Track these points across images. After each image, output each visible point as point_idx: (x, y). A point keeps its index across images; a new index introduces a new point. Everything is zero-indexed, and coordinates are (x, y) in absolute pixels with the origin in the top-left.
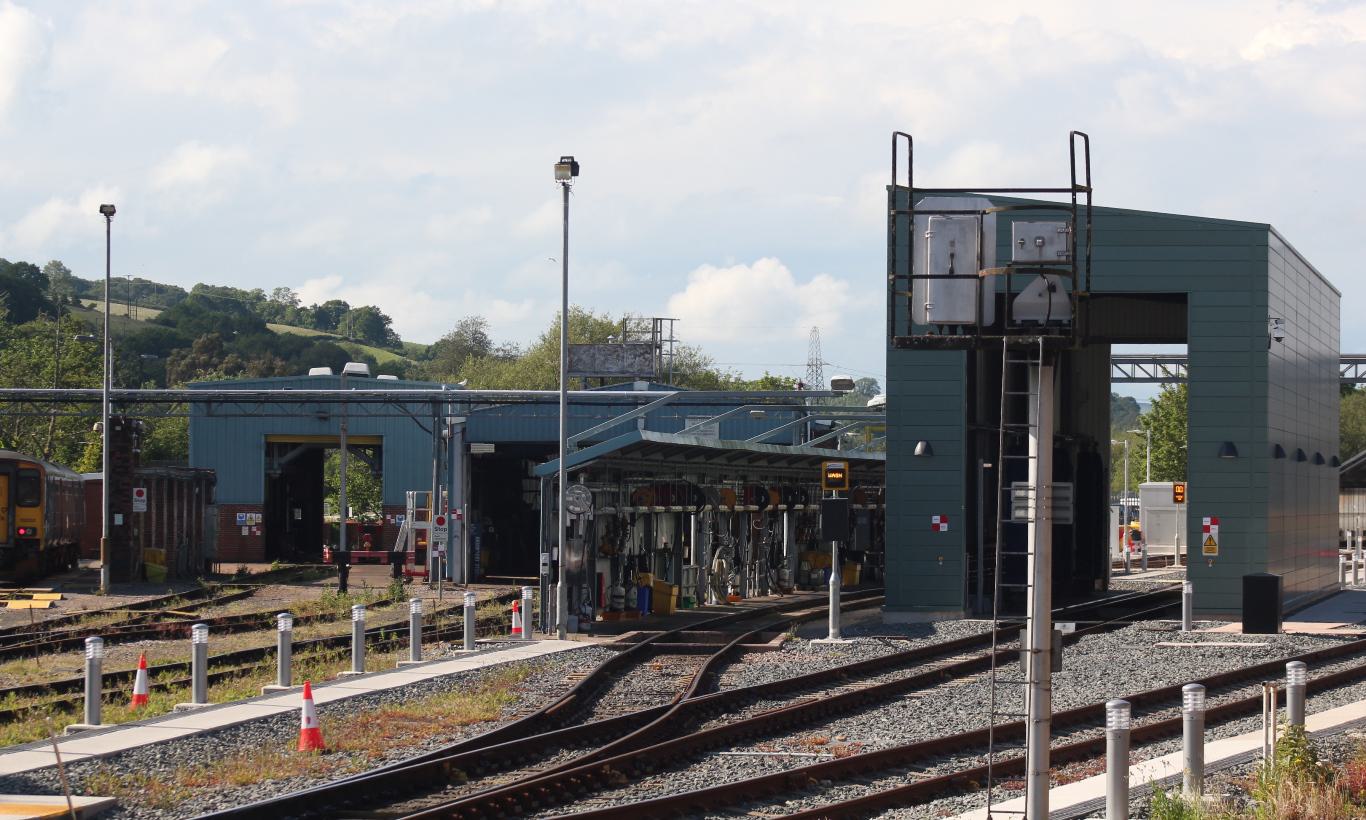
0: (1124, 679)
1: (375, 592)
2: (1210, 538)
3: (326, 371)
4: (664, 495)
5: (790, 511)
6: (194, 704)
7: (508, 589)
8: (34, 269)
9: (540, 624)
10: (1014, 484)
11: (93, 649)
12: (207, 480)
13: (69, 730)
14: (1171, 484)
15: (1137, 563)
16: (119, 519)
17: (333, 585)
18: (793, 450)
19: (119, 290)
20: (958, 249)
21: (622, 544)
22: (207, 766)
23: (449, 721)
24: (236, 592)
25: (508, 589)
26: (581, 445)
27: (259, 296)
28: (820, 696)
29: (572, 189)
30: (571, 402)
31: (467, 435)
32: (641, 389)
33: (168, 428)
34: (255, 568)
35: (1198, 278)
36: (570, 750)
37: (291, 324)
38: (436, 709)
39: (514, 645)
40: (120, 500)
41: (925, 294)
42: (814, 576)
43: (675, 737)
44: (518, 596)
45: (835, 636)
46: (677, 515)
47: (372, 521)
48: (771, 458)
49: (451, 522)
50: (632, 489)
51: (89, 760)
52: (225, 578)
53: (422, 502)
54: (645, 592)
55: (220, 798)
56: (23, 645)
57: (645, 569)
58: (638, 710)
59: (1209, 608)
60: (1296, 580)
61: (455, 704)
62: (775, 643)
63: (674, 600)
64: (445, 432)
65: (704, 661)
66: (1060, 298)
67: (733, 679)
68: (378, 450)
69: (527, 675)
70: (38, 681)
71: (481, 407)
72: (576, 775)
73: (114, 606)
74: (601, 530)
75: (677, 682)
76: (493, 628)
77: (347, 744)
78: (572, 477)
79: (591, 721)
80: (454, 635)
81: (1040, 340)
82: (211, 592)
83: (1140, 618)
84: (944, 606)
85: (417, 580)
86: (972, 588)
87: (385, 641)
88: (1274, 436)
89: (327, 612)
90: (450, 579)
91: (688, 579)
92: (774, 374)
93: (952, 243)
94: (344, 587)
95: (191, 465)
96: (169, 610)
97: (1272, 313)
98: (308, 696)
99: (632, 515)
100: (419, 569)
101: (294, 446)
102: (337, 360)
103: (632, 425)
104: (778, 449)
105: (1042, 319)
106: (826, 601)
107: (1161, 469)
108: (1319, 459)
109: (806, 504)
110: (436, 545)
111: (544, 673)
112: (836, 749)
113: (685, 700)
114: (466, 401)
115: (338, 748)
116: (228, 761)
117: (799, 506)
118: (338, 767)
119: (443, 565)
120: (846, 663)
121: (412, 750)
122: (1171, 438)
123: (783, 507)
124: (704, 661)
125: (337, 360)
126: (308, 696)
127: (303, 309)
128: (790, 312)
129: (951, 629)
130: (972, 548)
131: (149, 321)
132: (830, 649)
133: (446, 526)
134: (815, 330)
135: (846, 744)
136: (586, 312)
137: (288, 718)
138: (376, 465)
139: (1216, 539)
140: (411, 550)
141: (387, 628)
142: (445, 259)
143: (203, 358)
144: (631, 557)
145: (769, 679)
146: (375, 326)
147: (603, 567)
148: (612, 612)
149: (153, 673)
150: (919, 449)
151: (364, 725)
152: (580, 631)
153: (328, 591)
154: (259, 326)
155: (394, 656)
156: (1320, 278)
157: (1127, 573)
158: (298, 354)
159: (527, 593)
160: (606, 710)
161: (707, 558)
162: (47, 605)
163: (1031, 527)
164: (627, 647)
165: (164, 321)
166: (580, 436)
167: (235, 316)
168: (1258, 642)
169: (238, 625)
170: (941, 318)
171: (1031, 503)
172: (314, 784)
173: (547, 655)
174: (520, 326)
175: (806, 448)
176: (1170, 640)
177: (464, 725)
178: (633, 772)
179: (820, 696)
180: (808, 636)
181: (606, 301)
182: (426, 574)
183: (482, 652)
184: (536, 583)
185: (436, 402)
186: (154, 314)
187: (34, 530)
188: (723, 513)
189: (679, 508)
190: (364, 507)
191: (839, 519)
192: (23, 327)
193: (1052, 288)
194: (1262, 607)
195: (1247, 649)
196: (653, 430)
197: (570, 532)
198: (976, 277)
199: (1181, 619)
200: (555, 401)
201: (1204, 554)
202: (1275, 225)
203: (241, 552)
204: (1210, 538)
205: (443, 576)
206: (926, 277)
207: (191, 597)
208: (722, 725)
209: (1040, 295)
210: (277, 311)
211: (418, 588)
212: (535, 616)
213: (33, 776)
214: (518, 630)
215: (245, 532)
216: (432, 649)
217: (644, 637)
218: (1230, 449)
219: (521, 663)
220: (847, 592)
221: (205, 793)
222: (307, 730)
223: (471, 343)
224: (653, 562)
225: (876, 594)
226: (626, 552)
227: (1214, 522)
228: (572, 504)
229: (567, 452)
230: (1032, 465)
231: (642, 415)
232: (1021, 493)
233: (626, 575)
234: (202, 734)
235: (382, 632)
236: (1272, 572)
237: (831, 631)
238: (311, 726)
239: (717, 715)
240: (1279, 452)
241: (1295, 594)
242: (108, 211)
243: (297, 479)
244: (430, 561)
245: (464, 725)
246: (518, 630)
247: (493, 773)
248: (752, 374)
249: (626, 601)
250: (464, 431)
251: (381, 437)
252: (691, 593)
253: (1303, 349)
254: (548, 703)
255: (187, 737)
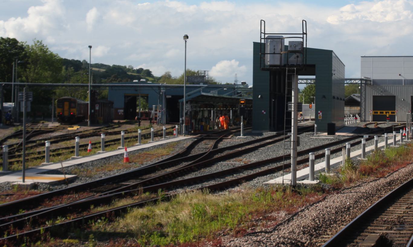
0: (304, 145)
1: (146, 126)
2: (320, 115)
3: (137, 81)
4: (206, 106)
5: (232, 110)
6: (101, 151)
7: (173, 126)
8: (80, 61)
9: (180, 133)
10: (289, 102)
11: (77, 140)
12: (112, 103)
13: (72, 158)
14: (309, 105)
15: (302, 120)
16: (93, 111)
17: (137, 125)
18: (233, 97)
19: (97, 65)
20: (276, 47)
21: (197, 117)
22: (102, 166)
23: (158, 155)
24: (117, 126)
25: (173, 126)
26: (189, 96)
27: (125, 67)
28: (240, 149)
29: (187, 42)
30: (186, 87)
31: (166, 94)
32: (201, 85)
33: (106, 92)
34: (122, 121)
35: (318, 62)
36: (185, 162)
37: (132, 72)
38: (156, 152)
39: (174, 138)
40: (93, 107)
41: (268, 58)
42: (237, 123)
43: (208, 159)
44: (175, 127)
45: (242, 136)
46: (209, 110)
47: (147, 112)
48: (228, 99)
49: (162, 112)
50: (199, 105)
51: (74, 165)
52: (115, 123)
53: (156, 107)
54: (202, 126)
55: (103, 174)
56: (68, 138)
57: (202, 121)
58: (202, 152)
59: (320, 130)
60: (338, 124)
61: (160, 151)
62: (230, 137)
63: (208, 128)
64: (161, 93)
65: (215, 141)
66: (299, 59)
67: (221, 145)
68: (147, 97)
69: (176, 144)
70: (69, 146)
71: (168, 88)
72: (186, 169)
73: (89, 129)
74: (193, 113)
75: (209, 146)
76: (170, 134)
77: (135, 161)
78: (187, 102)
79: (190, 155)
80: (161, 135)
81: (295, 69)
82: (112, 126)
83: (306, 132)
84: (266, 130)
85: (155, 124)
86: (270, 125)
87: (146, 137)
88: (333, 94)
89: (135, 130)
90: (162, 123)
91: (211, 124)
92: (228, 83)
93: (274, 46)
94: (139, 125)
95: (109, 100)
96: (102, 130)
97: (333, 69)
98: (126, 150)
99: (199, 110)
100: (155, 121)
101: (130, 96)
102: (139, 79)
103: (200, 91)
104: (230, 97)
105: (295, 64)
106: (240, 128)
107: (306, 101)
108: (341, 99)
109: (235, 108)
110: (159, 116)
111: (180, 144)
112: (244, 162)
113: (211, 150)
114: (166, 87)
115: (133, 162)
116: (107, 165)
117: (234, 109)
118: (132, 166)
119: (160, 121)
120: (245, 142)
121: (149, 162)
122: (308, 95)
123: (231, 109)
124: (215, 141)
125: (139, 79)
126: (126, 150)
127: (134, 70)
128: (232, 69)
129: (266, 134)
130: (270, 117)
131: (103, 72)
132: (241, 138)
133: (161, 112)
134: (236, 74)
135: (247, 160)
136: (190, 70)
137: (122, 155)
138: (147, 101)
139: (321, 115)
140: (154, 117)
141: (147, 134)
142: (164, 62)
143: (114, 79)
144: (199, 119)
145: (228, 145)
146: (148, 73)
147: (193, 121)
148: (195, 131)
149: (92, 144)
150: (259, 96)
151: (139, 156)
152: (188, 134)
153: (136, 126)
154: (126, 73)
155: (148, 140)
156: (341, 62)
157: (300, 122)
158: (134, 78)
159: (177, 127)
160: (195, 152)
161: (215, 119)
162: (76, 129)
163: (293, 113)
164: (198, 138)
165: (105, 72)
166: (189, 93)
167: (121, 71)
168: (331, 137)
169: (111, 134)
170: (272, 63)
171: (293, 107)
172: (126, 171)
173: (181, 139)
174: (177, 73)
175: (235, 97)
176: (312, 136)
177: (162, 156)
178: (199, 167)
179: (240, 149)
180: (236, 135)
181: (194, 68)
182: (157, 122)
183: (167, 139)
184: (179, 124)
185: (159, 87)
186: (104, 70)
187: (74, 113)
188: (218, 110)
189: (209, 109)
190: (145, 109)
191: (242, 111)
192: (77, 73)
193: (298, 57)
194: (331, 130)
195: (329, 139)
196: (204, 92)
197: (186, 114)
198: (280, 54)
199: (314, 132)
200: (183, 87)
201: (319, 119)
202: (334, 51)
203: (119, 118)
204: (320, 115)
205: (160, 123)
206: (268, 54)
207: (107, 127)
208: (234, 178)
209: (295, 58)
210: (129, 70)
211: (155, 125)
212: (179, 131)
213: (59, 170)
214: (175, 134)
215: (120, 114)
216: (157, 139)
217: (202, 136)
218: (324, 97)
219: (175, 142)
220: (244, 126)
221: (100, 173)
222: (126, 158)
223: (168, 76)
224: (204, 120)
225: (252, 127)
226: (198, 118)
227: (321, 112)
228: (186, 108)
229: (185, 97)
230: (293, 98)
231: (201, 89)
232: (290, 105)
233: (198, 122)
234: (102, 159)
235: (146, 135)
236: (333, 122)
237: (241, 135)
238: (127, 157)
239: (218, 154)
240: (334, 97)
241: (337, 127)
242: (90, 47)
243: (131, 103)
244: (158, 119)
245: (162, 156)
246: (175, 134)
247: (167, 168)
248: (224, 83)
249: (199, 128)
250: (165, 93)
251: (148, 94)
252: (212, 127)
253: (338, 77)
254: (181, 151)
255: (98, 159)
